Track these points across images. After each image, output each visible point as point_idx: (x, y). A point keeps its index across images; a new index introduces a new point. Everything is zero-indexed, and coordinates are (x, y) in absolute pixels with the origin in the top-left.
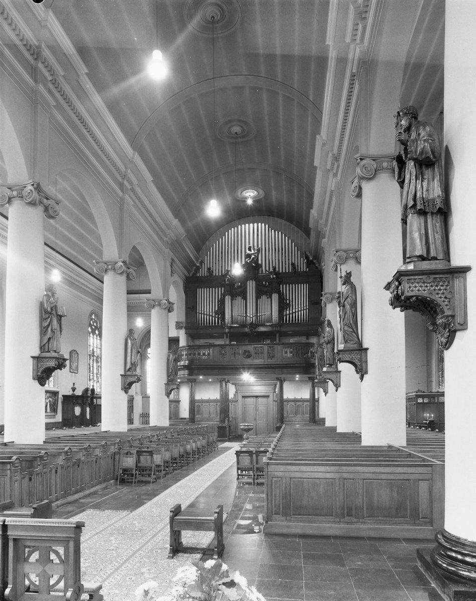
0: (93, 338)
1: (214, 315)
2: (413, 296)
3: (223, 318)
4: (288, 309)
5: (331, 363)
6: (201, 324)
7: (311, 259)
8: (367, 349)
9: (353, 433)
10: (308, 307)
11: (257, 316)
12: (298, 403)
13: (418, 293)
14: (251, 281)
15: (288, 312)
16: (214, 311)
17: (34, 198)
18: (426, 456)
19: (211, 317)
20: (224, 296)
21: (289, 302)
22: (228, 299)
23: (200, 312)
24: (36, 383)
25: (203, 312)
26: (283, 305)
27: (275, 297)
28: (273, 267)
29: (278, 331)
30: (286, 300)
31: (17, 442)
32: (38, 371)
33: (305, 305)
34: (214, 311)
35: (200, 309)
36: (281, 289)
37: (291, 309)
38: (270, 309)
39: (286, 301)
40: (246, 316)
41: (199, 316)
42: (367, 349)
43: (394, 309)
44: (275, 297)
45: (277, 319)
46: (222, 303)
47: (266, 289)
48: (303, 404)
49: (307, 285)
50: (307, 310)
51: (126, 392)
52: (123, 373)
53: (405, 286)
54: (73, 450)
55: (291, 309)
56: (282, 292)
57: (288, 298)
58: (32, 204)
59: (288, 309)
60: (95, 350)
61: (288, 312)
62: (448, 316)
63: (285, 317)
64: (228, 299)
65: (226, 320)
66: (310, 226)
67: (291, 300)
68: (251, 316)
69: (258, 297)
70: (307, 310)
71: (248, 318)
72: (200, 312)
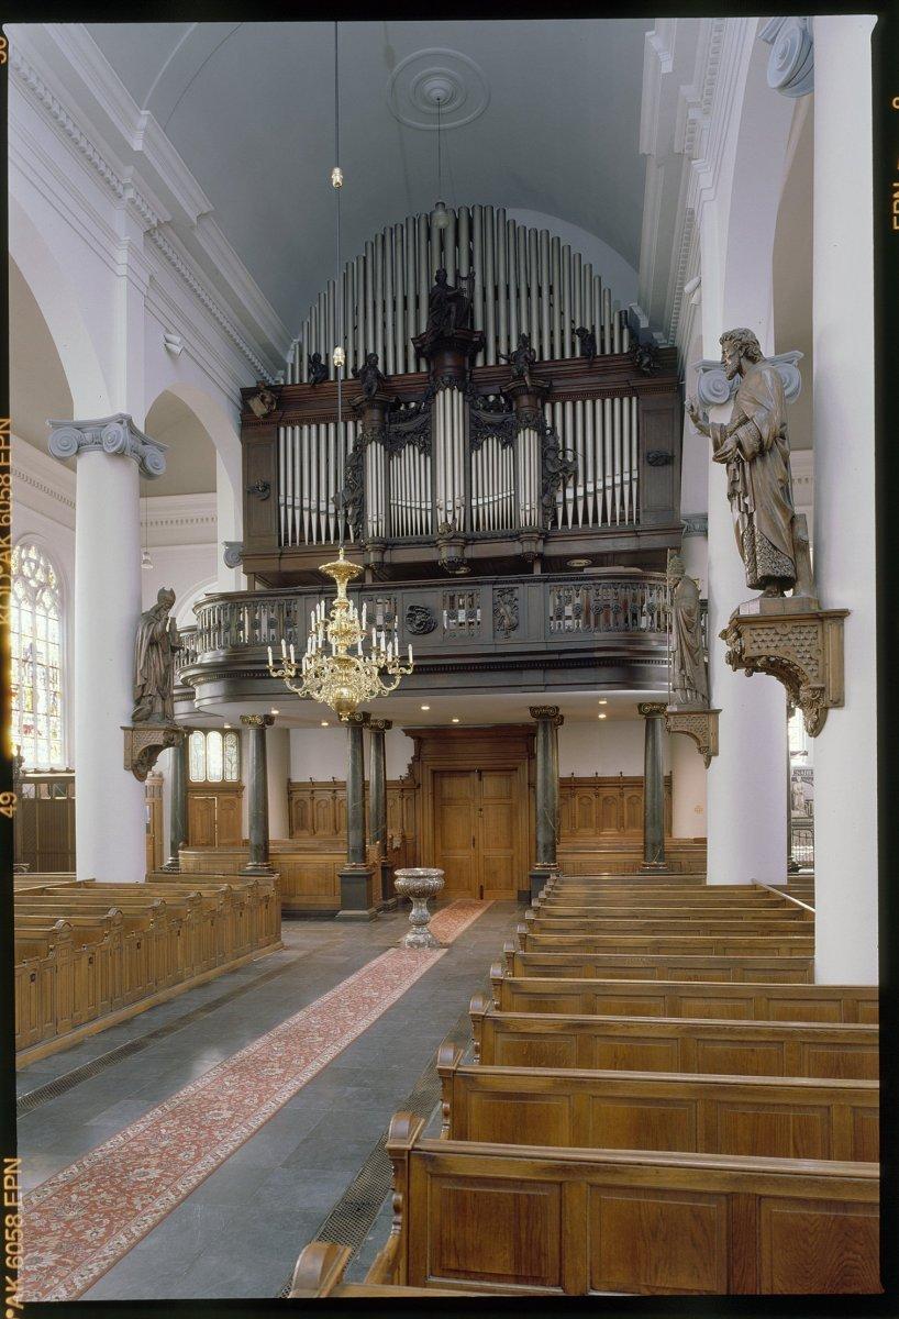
0: (33, 613)
1: (332, 510)
2: (760, 657)
3: (361, 517)
4: (571, 483)
5: (780, 572)
6: (294, 541)
7: (644, 324)
8: (717, 712)
9: (754, 887)
10: (635, 475)
11: (468, 508)
12: (606, 792)
13: (772, 652)
14: (448, 391)
15: (570, 494)
16: (332, 495)
17: (122, 446)
18: (797, 906)
19: (323, 518)
20: (360, 448)
21: (575, 459)
22: (374, 452)
23: (289, 501)
24: (130, 776)
25: (297, 503)
26: (556, 470)
27: (528, 441)
28: (520, 337)
29: (540, 557)
30: (565, 450)
31: (100, 880)
32: (132, 754)
33: (626, 468)
34: (332, 495)
35: (290, 493)
36: (548, 417)
37: (580, 482)
38: (507, 482)
39: (564, 456)
40: (435, 508)
41: (288, 517)
42: (717, 712)
43: (735, 670)
44: (528, 441)
45: (535, 513)
46: (356, 466)
47: (497, 418)
48: (622, 795)
49: (634, 399)
50: (635, 484)
51: (141, 777)
52: (128, 724)
53: (746, 640)
54: (204, 895)
55: (580, 482)
56: (549, 424)
57: (569, 445)
58: (120, 454)
59: (571, 483)
60: (40, 647)
61: (570, 494)
62: (814, 689)
63: (560, 511)
64: (374, 452)
65: (370, 524)
66: (644, 149)
67: (580, 450)
68: (450, 507)
69: (474, 442)
70: (635, 484)
71: (441, 515)
72: (289, 501)
